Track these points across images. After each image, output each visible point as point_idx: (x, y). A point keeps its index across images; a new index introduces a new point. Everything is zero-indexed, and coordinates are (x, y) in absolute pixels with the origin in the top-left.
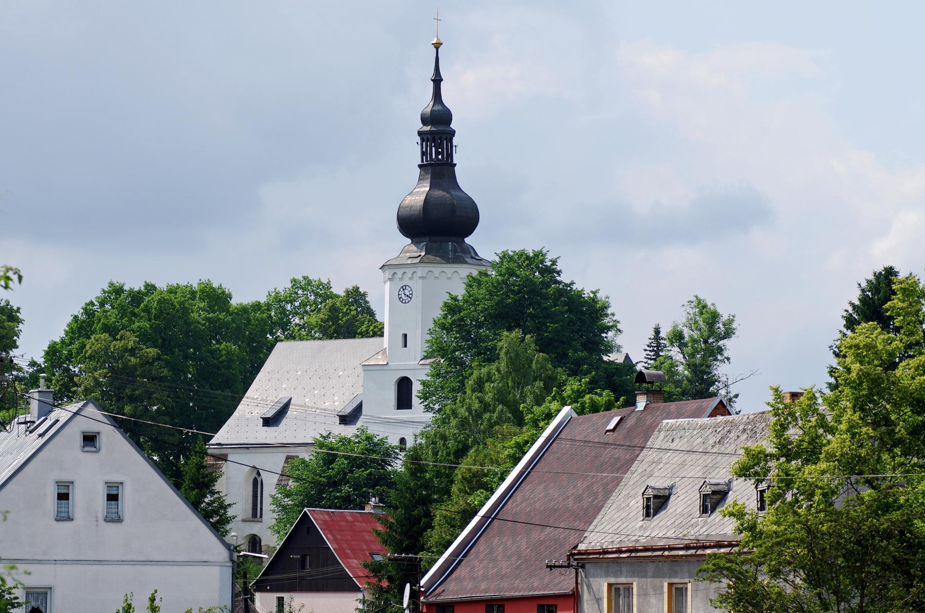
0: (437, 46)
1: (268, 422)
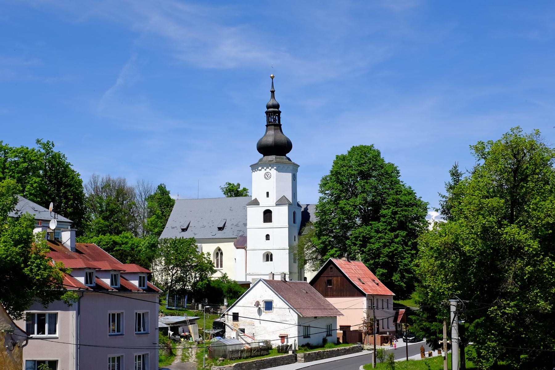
0: (272, 78)
1: (220, 229)
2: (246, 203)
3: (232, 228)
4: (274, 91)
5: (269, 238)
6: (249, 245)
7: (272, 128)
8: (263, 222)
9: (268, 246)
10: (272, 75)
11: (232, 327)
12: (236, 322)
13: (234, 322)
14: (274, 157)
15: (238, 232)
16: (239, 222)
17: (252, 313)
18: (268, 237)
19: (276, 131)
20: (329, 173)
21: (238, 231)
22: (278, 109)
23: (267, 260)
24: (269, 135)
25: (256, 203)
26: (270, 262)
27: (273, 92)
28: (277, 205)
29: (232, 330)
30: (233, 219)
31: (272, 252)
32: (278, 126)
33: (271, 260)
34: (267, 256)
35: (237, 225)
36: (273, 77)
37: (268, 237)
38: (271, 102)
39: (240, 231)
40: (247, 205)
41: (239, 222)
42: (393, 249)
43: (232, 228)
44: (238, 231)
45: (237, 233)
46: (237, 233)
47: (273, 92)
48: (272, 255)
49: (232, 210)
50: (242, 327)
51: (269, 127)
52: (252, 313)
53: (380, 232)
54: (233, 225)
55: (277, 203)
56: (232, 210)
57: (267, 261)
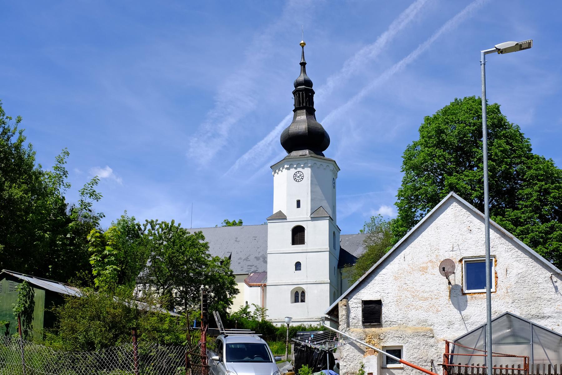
0: (303, 45)
2: (267, 217)
3: (240, 263)
4: (305, 63)
5: (300, 267)
6: (270, 280)
7: (304, 112)
8: (291, 244)
9: (299, 278)
10: (302, 42)
11: (363, 344)
12: (373, 329)
13: (367, 330)
14: (308, 152)
15: (249, 267)
16: (250, 255)
17: (426, 299)
18: (298, 266)
19: (309, 116)
20: (417, 138)
21: (249, 266)
22: (312, 88)
23: (296, 301)
24: (300, 122)
25: (281, 217)
26: (300, 304)
27: (303, 64)
28: (313, 219)
29: (363, 352)
30: (241, 252)
31: (304, 287)
32: (311, 112)
33: (303, 301)
34: (297, 293)
35: (247, 259)
36: (304, 44)
37: (298, 266)
38: (302, 78)
39: (251, 266)
40: (268, 220)
41: (250, 255)
42: (551, 248)
43: (240, 263)
44: (249, 266)
45: (248, 269)
46: (248, 269)
47: (303, 64)
48: (303, 293)
49: (239, 241)
50: (391, 343)
51: (298, 111)
52: (426, 299)
53: (522, 224)
54: (240, 259)
55: (312, 216)
56: (239, 241)
57: (295, 302)
